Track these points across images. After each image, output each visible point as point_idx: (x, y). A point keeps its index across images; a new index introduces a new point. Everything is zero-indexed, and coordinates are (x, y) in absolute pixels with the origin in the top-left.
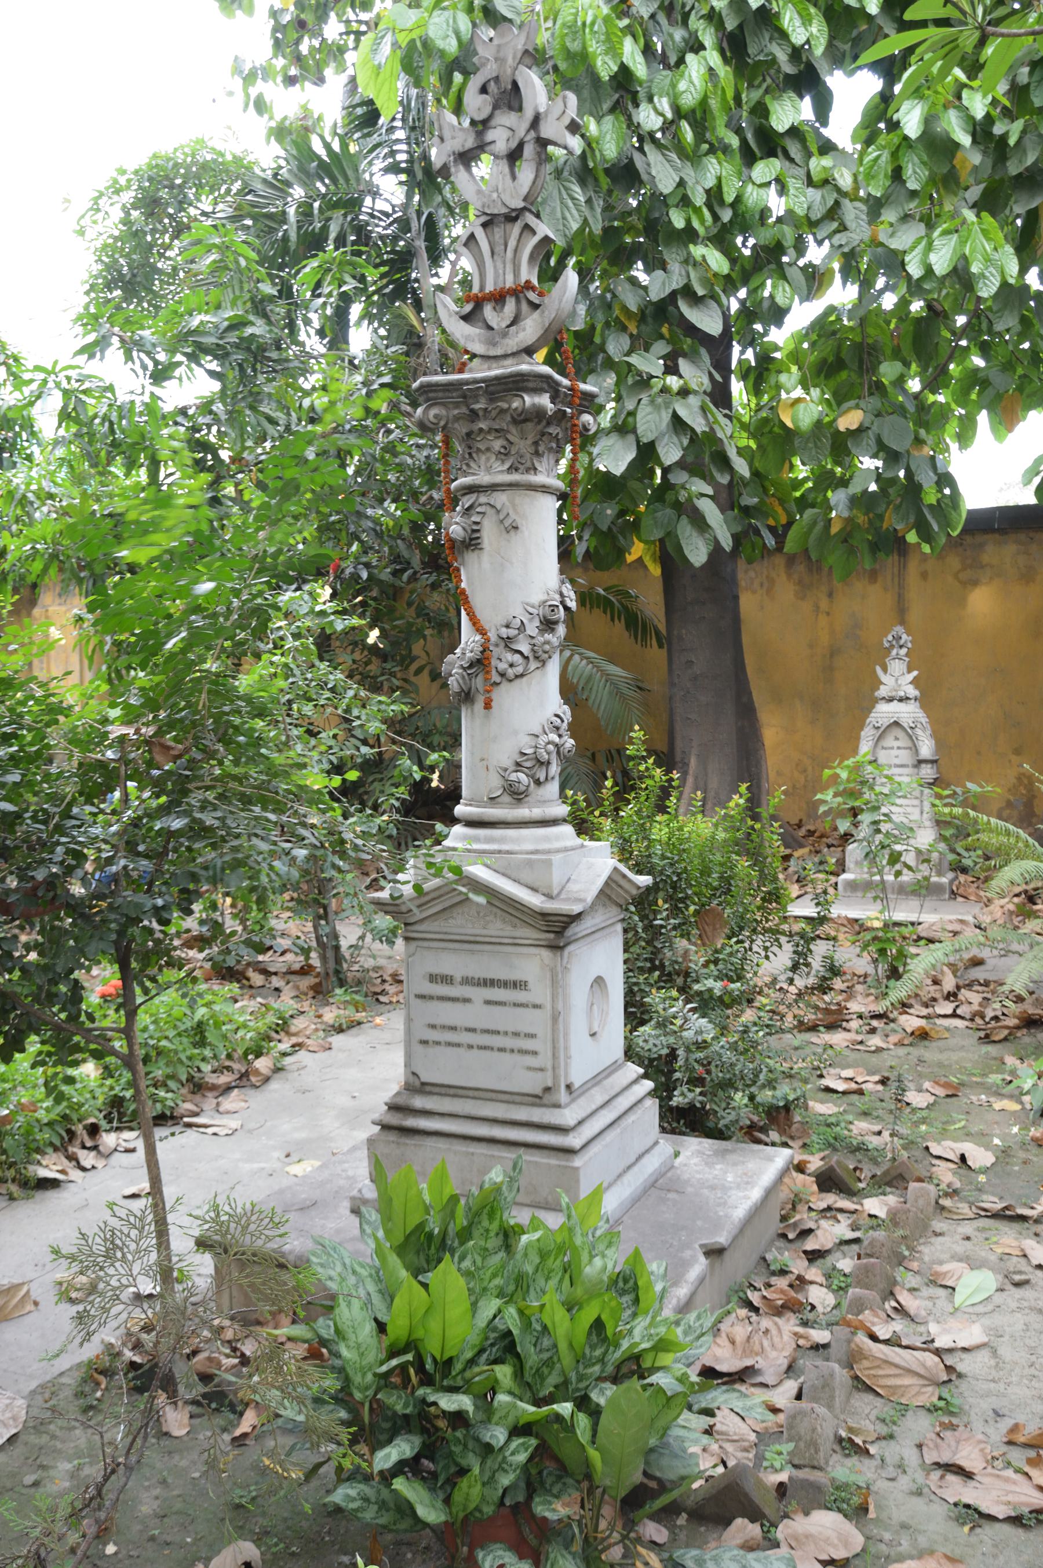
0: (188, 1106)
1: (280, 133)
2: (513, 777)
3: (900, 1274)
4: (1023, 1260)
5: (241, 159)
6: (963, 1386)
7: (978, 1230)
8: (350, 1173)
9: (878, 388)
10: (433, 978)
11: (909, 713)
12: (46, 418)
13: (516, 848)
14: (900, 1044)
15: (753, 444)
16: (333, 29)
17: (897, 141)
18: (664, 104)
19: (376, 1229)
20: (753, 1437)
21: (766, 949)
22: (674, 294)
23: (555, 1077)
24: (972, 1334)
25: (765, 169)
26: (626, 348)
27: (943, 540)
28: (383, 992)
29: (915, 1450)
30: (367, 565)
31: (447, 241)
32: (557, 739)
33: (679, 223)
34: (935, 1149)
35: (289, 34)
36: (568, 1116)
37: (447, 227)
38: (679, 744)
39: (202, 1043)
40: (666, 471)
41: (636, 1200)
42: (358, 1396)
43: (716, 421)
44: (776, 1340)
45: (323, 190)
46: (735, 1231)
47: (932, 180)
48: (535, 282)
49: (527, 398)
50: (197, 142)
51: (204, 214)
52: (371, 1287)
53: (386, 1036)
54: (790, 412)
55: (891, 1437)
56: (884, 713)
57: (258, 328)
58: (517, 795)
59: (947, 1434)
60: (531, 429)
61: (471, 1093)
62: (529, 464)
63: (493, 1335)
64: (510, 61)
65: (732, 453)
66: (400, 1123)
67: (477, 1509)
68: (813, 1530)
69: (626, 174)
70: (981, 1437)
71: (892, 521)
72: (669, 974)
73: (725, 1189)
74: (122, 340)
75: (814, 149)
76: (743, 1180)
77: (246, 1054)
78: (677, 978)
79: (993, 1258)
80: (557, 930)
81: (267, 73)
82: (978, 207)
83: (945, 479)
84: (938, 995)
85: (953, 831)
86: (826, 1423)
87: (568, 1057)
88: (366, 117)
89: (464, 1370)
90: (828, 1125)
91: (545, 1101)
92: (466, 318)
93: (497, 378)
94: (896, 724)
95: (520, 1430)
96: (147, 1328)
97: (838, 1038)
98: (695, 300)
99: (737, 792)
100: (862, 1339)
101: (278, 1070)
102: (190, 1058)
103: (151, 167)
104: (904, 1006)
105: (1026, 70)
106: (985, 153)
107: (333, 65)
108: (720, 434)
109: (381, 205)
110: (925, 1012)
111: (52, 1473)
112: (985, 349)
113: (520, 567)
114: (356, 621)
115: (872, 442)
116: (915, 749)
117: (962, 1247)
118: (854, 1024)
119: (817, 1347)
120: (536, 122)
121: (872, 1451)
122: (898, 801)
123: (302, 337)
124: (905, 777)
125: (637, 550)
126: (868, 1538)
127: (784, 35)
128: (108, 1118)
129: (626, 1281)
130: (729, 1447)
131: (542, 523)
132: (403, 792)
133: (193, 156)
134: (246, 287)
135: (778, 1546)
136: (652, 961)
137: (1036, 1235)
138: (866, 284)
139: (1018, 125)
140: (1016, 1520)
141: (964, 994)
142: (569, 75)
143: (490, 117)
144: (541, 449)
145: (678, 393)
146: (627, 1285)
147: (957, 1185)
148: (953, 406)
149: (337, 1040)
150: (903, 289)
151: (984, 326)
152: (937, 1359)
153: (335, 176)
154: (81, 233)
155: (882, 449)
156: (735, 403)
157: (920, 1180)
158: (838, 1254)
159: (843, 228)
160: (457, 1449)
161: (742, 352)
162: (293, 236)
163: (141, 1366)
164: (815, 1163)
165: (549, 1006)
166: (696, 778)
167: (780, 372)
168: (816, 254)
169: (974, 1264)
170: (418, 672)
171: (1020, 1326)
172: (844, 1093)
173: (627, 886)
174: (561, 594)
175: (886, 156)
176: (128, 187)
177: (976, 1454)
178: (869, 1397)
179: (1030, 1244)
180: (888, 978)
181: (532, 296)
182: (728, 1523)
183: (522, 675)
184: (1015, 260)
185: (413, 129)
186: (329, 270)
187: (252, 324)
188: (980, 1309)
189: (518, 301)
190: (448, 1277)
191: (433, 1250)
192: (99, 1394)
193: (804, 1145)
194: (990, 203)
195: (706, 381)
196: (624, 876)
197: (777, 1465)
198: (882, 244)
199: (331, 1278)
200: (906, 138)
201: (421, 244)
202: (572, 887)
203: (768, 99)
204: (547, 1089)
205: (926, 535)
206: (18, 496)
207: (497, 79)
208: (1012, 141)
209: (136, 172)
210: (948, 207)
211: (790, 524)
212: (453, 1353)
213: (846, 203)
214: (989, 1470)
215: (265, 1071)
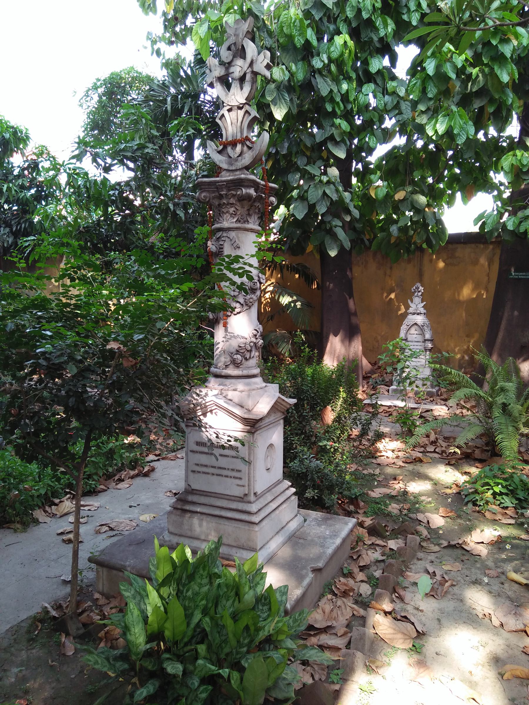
0: (102, 487)
2: (235, 357)
11: (420, 319)
15: (360, 204)
18: (325, 57)
23: (249, 490)
26: (305, 163)
33: (329, 108)
35: (170, 23)
36: (254, 508)
40: (322, 215)
44: (344, 611)
56: (412, 319)
60: (246, 204)
61: (213, 495)
64: (241, 36)
65: (352, 208)
69: (308, 86)
72: (308, 437)
82: (458, 105)
84: (427, 442)
85: (438, 375)
87: (255, 481)
90: (377, 503)
92: (220, 152)
93: (231, 181)
103: (110, 78)
105: (480, 46)
110: (422, 449)
111: (8, 673)
116: (423, 334)
120: (251, 64)
125: (310, 248)
129: (265, 600)
137: (462, 561)
143: (232, 61)
144: (251, 212)
145: (326, 183)
148: (446, 189)
151: (460, 155)
154: (81, 105)
159: (400, 113)
161: (357, 165)
164: (368, 522)
171: (451, 608)
174: (259, 277)
175: (419, 82)
184: (474, 128)
187: (148, 147)
192: (36, 632)
193: (365, 512)
196: (284, 400)
204: (246, 495)
206: (50, 217)
207: (235, 44)
209: (104, 80)
213: (402, 102)
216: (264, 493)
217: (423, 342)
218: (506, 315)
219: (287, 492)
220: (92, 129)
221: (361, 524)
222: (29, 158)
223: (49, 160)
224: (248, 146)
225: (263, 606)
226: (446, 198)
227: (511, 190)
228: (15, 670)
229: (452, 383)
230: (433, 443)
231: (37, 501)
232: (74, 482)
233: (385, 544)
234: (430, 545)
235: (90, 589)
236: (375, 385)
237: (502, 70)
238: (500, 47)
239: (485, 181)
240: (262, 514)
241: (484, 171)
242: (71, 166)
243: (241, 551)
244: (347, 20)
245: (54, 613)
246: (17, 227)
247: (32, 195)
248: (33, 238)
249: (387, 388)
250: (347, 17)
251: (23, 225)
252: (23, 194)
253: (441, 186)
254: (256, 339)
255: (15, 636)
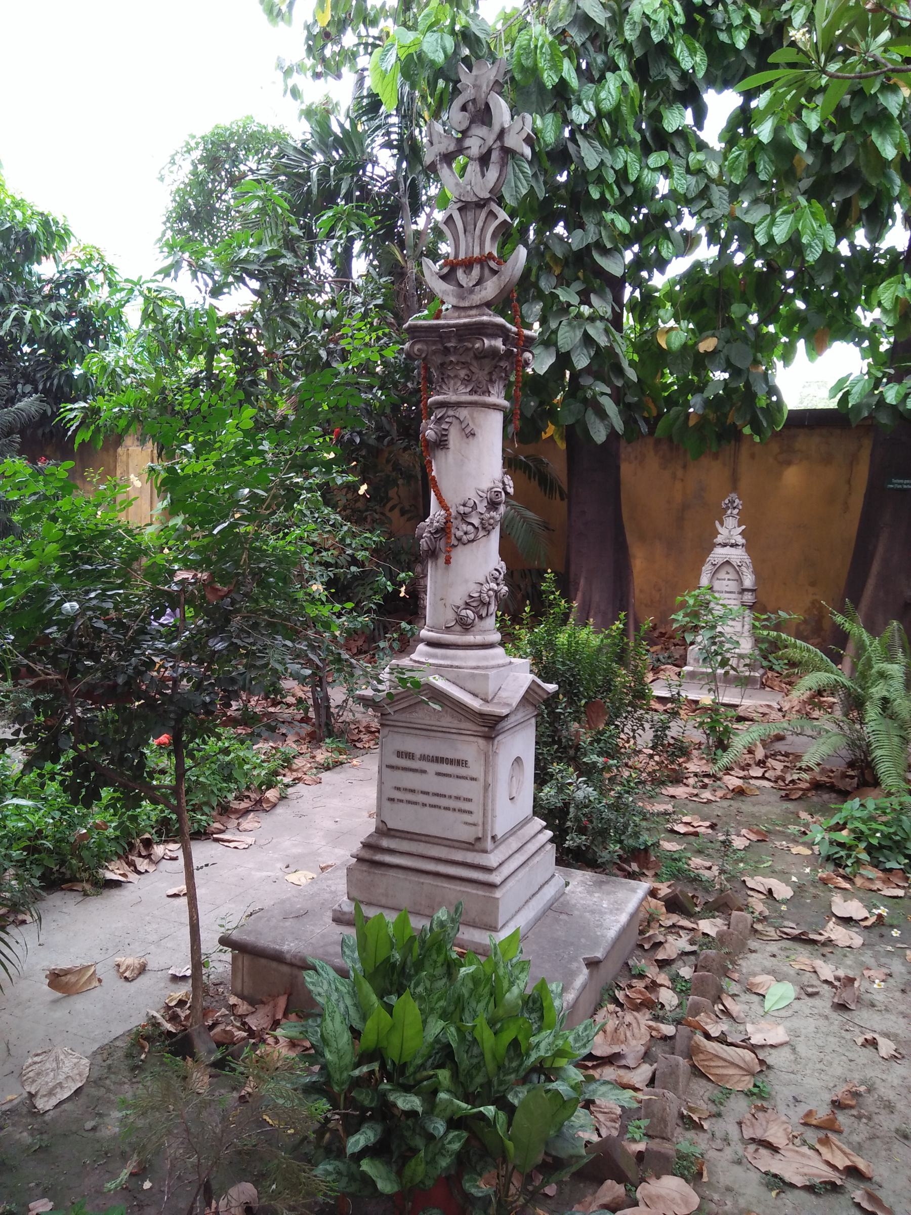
0: (217, 825)
1: (309, 113)
2: (463, 613)
3: (725, 982)
4: (813, 975)
5: (279, 132)
6: (771, 1075)
7: (781, 949)
8: (333, 888)
9: (729, 322)
10: (400, 754)
11: (737, 555)
12: (133, 314)
13: (463, 664)
14: (723, 798)
16: (349, 39)
17: (752, 144)
19: (353, 951)
20: (619, 1111)
21: (634, 731)
22: (588, 247)
24: (777, 1035)
25: (656, 159)
26: (554, 284)
27: (769, 434)
28: (360, 740)
29: (736, 1127)
30: (360, 433)
31: (424, 198)
32: (496, 587)
33: (596, 195)
34: (750, 883)
35: (319, 40)
36: (492, 860)
37: (424, 187)
38: (573, 568)
39: (229, 778)
41: (538, 919)
42: (336, 1089)
43: (615, 340)
44: (636, 1031)
45: (337, 157)
46: (608, 949)
47: (776, 174)
48: (495, 254)
49: (486, 341)
50: (247, 118)
51: (251, 170)
52: (349, 1001)
53: (360, 774)
54: (665, 337)
55: (719, 1115)
56: (719, 554)
57: (288, 260)
58: (465, 626)
59: (760, 1115)
60: (488, 364)
61: (423, 838)
62: (484, 388)
63: (437, 1046)
64: (484, 88)
65: (625, 364)
66: (372, 858)
67: (422, 1182)
68: (663, 1192)
69: (560, 156)
70: (784, 1118)
71: (733, 418)
72: (565, 747)
73: (602, 913)
74: (190, 265)
75: (694, 147)
76: (614, 906)
77: (260, 786)
78: (570, 753)
79: (792, 972)
80: (490, 726)
81: (301, 68)
83: (773, 390)
84: (751, 762)
85: (768, 649)
86: (672, 1102)
87: (494, 816)
88: (373, 105)
89: (415, 1073)
90: (675, 860)
91: (476, 848)
92: (444, 278)
94: (728, 562)
95: (455, 1123)
96: (181, 1003)
97: (680, 791)
98: (605, 252)
99: (618, 619)
100: (699, 1038)
101: (283, 798)
102: (220, 790)
103: (213, 134)
104: (728, 770)
106: (816, 156)
107: (348, 65)
108: (618, 350)
109: (379, 171)
110: (742, 773)
111: (106, 1119)
112: (805, 297)
113: (475, 463)
114: (351, 478)
115: (723, 361)
116: (740, 581)
117: (769, 963)
118: (691, 781)
119: (665, 1038)
121: (706, 1127)
122: (730, 623)
123: (318, 263)
124: (733, 602)
126: (702, 1198)
127: (675, 63)
128: (159, 833)
129: (534, 1002)
130: (601, 1117)
131: (491, 431)
132: (378, 599)
133: (244, 127)
134: (280, 229)
135: (637, 1204)
136: (552, 737)
137: (823, 955)
138: (725, 246)
139: (840, 138)
140: (810, 1189)
141: (771, 762)
142: (522, 83)
143: (468, 129)
144: (494, 377)
145: (588, 319)
146: (535, 1004)
147: (767, 913)
148: (780, 335)
149: (325, 776)
150: (750, 249)
151: (806, 280)
152: (753, 1055)
153: (349, 149)
154: (162, 179)
155: (727, 366)
156: (625, 327)
157: (741, 910)
158: (680, 963)
159: (710, 205)
160: (408, 1134)
162: (315, 190)
163: (175, 1035)
164: (664, 890)
165: (482, 780)
166: (584, 594)
167: (659, 308)
168: (689, 223)
169: (780, 978)
170: (391, 509)
171: (812, 1029)
172: (684, 834)
173: (540, 692)
174: (503, 483)
176: (197, 148)
177: (781, 1133)
178: (703, 1082)
179: (819, 963)
180: (717, 748)
181: (492, 264)
182: (601, 1182)
183: (473, 541)
185: (404, 117)
186: (340, 219)
188: (783, 1013)
189: (482, 268)
190: (407, 1006)
191: (395, 977)
192: (143, 1056)
193: (656, 875)
194: (816, 193)
195: (609, 310)
196: (539, 686)
197: (637, 1137)
198: (738, 218)
199: (319, 994)
200: (760, 142)
201: (406, 201)
202: (502, 694)
203: (662, 108)
204: (478, 839)
205: (757, 428)
206: (109, 370)
207: (474, 101)
208: (836, 149)
210: (787, 194)
211: (660, 415)
212: (408, 1060)
213: (714, 187)
214: (791, 1146)
215: (273, 799)
216: (506, 837)
217: (740, 593)
218: (881, 549)
219: (540, 836)
220: (180, 220)
221: (653, 893)
222: (68, 267)
223: (102, 270)
224: (491, 269)
225: (530, 1013)
226: (779, 350)
227: (892, 340)
228: (116, 1114)
229: (792, 664)
230: (761, 763)
231: (110, 848)
232: (174, 817)
233: (694, 926)
234: (768, 929)
235: (221, 990)
236: (657, 664)
237: (884, 138)
238: (881, 99)
239: (847, 323)
240: (506, 870)
241: (846, 306)
242: (153, 286)
243: (471, 930)
244: (626, 47)
245: (169, 1027)
246: (45, 385)
247: (72, 329)
248: (82, 404)
249: (678, 670)
250: (626, 40)
251: (56, 382)
252: (58, 328)
253: (771, 329)
254: (498, 584)
255: (109, 1062)
